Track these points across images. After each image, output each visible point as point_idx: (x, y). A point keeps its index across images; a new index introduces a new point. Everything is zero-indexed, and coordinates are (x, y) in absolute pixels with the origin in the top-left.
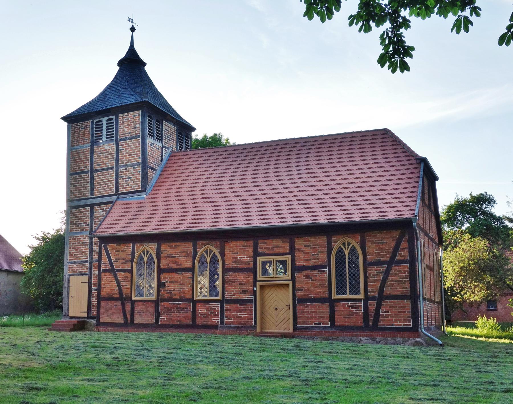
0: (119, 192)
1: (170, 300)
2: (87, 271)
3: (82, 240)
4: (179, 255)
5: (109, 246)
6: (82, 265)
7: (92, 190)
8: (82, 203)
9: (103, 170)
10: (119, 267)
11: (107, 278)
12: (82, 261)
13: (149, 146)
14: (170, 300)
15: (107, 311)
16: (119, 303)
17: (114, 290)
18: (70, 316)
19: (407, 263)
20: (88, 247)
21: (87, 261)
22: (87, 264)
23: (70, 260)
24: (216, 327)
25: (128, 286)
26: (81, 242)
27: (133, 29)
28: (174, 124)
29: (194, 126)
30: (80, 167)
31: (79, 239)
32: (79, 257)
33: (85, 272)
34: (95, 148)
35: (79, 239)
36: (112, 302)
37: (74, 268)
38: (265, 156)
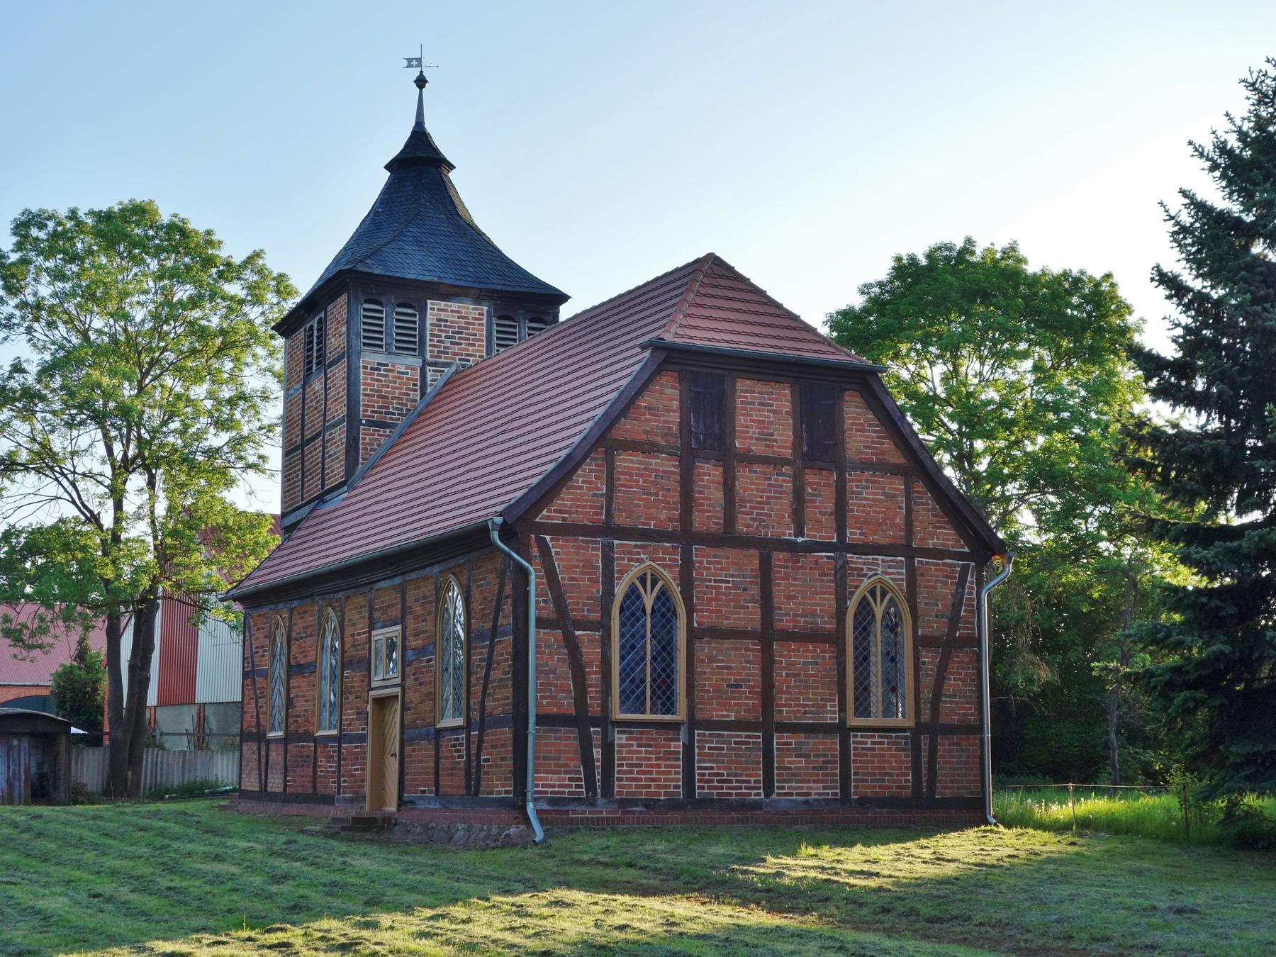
27: (421, 82)
28: (478, 300)
29: (564, 289)
38: (617, 342)
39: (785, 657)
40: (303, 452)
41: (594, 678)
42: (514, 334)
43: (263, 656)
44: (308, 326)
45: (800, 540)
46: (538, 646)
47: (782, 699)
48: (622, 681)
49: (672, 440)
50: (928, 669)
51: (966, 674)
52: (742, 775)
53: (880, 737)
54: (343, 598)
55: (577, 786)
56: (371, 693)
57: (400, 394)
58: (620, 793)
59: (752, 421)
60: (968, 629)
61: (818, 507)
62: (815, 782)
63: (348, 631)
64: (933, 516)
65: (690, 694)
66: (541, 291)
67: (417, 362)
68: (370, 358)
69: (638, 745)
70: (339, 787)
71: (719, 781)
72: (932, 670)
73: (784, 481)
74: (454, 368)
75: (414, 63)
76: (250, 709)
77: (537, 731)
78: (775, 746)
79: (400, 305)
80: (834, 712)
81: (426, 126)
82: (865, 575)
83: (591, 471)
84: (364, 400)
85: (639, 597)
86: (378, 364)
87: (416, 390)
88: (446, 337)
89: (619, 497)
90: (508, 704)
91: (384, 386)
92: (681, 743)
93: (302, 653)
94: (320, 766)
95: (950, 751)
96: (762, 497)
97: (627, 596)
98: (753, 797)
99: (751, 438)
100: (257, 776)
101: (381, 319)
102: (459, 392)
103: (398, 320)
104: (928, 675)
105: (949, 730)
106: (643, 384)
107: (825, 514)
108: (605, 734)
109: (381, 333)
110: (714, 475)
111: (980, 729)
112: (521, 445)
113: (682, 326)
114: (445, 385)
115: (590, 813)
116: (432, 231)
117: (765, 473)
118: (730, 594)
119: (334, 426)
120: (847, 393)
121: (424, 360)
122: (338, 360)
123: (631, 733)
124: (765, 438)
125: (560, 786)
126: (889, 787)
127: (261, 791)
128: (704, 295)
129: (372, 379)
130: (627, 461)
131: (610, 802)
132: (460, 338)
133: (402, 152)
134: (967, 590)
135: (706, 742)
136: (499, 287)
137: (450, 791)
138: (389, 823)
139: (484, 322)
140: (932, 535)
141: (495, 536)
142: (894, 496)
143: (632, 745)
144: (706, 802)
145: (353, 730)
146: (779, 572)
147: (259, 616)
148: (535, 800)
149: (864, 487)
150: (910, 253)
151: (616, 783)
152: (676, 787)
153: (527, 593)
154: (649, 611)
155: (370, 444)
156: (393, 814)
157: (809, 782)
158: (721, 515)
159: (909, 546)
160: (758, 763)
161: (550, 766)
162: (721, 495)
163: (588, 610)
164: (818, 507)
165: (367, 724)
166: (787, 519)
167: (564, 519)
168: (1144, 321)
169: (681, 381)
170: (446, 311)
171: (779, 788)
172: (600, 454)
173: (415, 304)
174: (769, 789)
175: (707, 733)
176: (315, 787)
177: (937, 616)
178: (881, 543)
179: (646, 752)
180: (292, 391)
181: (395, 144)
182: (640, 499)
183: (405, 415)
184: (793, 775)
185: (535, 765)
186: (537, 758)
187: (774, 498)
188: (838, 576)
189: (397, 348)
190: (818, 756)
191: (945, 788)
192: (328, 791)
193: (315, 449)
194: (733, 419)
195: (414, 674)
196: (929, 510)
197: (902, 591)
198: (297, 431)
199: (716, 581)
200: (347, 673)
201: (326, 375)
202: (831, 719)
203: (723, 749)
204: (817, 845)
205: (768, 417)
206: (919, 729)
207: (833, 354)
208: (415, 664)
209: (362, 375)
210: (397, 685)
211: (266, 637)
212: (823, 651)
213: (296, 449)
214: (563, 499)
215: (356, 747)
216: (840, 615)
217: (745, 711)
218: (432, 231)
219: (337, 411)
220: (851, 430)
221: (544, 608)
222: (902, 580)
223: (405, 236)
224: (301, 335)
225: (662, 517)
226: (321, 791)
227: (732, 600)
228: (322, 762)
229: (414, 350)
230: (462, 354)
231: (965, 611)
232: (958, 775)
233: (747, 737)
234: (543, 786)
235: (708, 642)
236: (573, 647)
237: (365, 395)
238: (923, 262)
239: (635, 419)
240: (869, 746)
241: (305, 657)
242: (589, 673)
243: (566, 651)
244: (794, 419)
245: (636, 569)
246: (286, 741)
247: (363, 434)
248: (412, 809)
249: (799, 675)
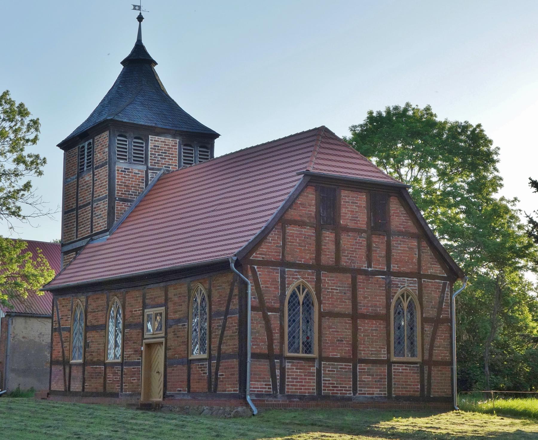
4: (98, 309)
13: (118, 173)
19: (237, 314)
24: (115, 395)
27: (140, 18)
28: (174, 136)
34: (81, 180)
39: (363, 326)
40: (77, 213)
41: (277, 336)
42: (192, 154)
43: (67, 320)
44: (81, 146)
45: (370, 269)
46: (252, 320)
47: (361, 347)
48: (289, 337)
49: (312, 220)
50: (427, 333)
51: (445, 336)
52: (343, 384)
53: (406, 366)
54: (124, 292)
55: (269, 388)
56: (144, 341)
57: (135, 184)
58: (288, 392)
59: (348, 211)
60: (446, 314)
61: (378, 254)
62: (376, 388)
63: (128, 309)
64: (431, 258)
65: (320, 345)
66: (205, 132)
67: (144, 168)
68: (121, 165)
69: (296, 369)
70: (122, 389)
71: (332, 387)
72: (429, 334)
73: (362, 240)
74: (162, 171)
75: (137, 8)
76: (58, 348)
77: (251, 361)
78: (358, 370)
79: (136, 138)
80: (385, 354)
81: (143, 42)
82: (399, 287)
83: (275, 234)
84: (117, 187)
85: (297, 296)
86: (125, 169)
87: (143, 183)
88: (158, 155)
89: (288, 247)
90: (236, 348)
91: (127, 180)
92: (315, 368)
93: (95, 319)
94: (109, 378)
95: (437, 373)
96: (353, 248)
97: (291, 296)
98: (348, 395)
99: (348, 219)
100: (63, 383)
101: (126, 145)
102: (169, 186)
103: (134, 146)
104: (427, 336)
105: (437, 363)
106: (300, 192)
107: (381, 257)
108: (281, 363)
109: (126, 152)
110: (331, 237)
111: (451, 363)
112: (226, 219)
113: (316, 164)
114: (158, 180)
115: (275, 401)
116: (150, 99)
117: (354, 237)
118: (338, 295)
119: (100, 200)
120: (392, 197)
121: (147, 167)
122: (102, 166)
123: (293, 363)
124: (354, 219)
125: (261, 388)
126: (409, 391)
127: (66, 390)
128: (323, 148)
129: (121, 177)
130: (291, 230)
131: (283, 396)
132: (165, 156)
133: (130, 56)
134: (445, 295)
135: (327, 368)
136: (185, 130)
137: (198, 390)
138: (159, 406)
139: (177, 147)
140: (430, 268)
141: (232, 265)
142: (412, 248)
143: (293, 369)
144: (327, 397)
145: (131, 359)
146: (360, 285)
147: (64, 299)
148: (251, 395)
149: (399, 244)
150: (378, 110)
151: (286, 387)
152: (313, 389)
153: (247, 294)
154: (301, 303)
155: (120, 211)
156: (160, 402)
157: (373, 388)
158: (334, 257)
159: (419, 273)
160: (350, 378)
161: (257, 378)
162: (334, 247)
163: (274, 303)
164: (378, 254)
165: (142, 356)
166: (364, 259)
167: (263, 258)
168: (499, 149)
169: (316, 190)
170: (158, 141)
171: (360, 391)
172: (279, 226)
173: (143, 138)
174: (355, 390)
175: (327, 363)
176: (105, 388)
177: (432, 308)
178: (406, 271)
179: (300, 372)
180: (69, 180)
181: (127, 51)
182: (297, 249)
183: (138, 195)
184: (366, 384)
185: (251, 378)
186: (251, 374)
187: (358, 248)
188: (387, 287)
189: (134, 160)
190: (377, 375)
191: (435, 392)
192: (114, 391)
193: (86, 211)
194: (340, 210)
195: (174, 332)
196: (428, 255)
197: (416, 295)
198: (73, 201)
199: (331, 289)
200: (126, 331)
201: (93, 173)
202: (383, 357)
203: (334, 371)
204: (397, 417)
205: (356, 209)
206: (424, 363)
207: (385, 178)
208: (174, 327)
209: (116, 174)
210: (162, 337)
211: (69, 310)
212: (380, 324)
213: (73, 210)
214: (263, 248)
215: (133, 368)
216: (388, 306)
217: (345, 353)
218: (150, 99)
219: (101, 192)
220: (393, 215)
221: (254, 301)
222: (416, 290)
223: (136, 101)
224: (76, 150)
225: (307, 257)
226: (109, 390)
227: (339, 299)
228: (110, 375)
229: (142, 161)
230: (166, 164)
231: (445, 305)
232: (441, 386)
233: (345, 365)
234: (253, 388)
235: (328, 319)
236: (267, 319)
237: (118, 185)
238: (384, 114)
239: (295, 209)
240: (401, 371)
241: (98, 321)
242: (275, 333)
243: (264, 322)
244: (367, 211)
245: (296, 283)
246: (84, 365)
247: (117, 205)
248: (172, 399)
249: (369, 336)
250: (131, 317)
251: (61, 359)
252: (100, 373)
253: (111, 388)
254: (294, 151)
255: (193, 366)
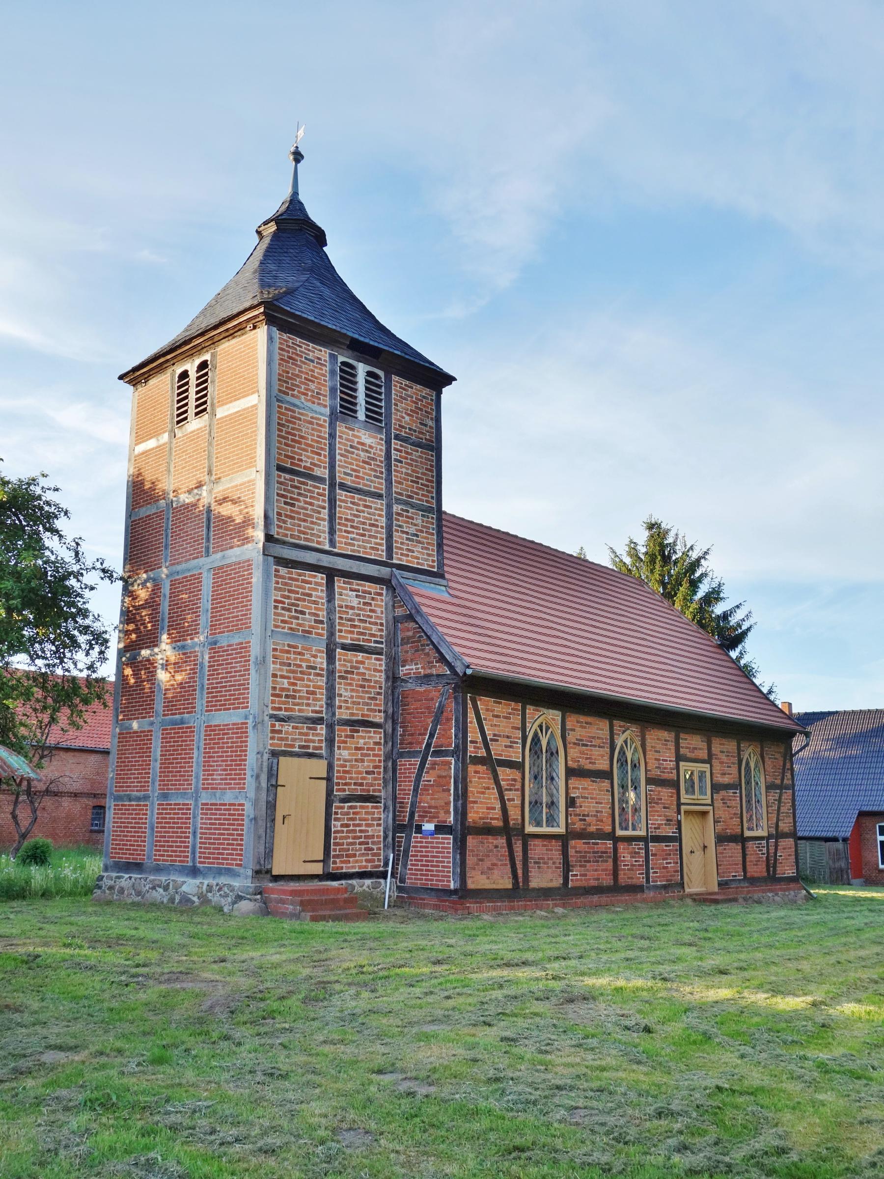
0: (395, 561)
1: (582, 835)
2: (321, 748)
3: (308, 661)
5: (480, 700)
6: (309, 728)
7: (332, 531)
8: (310, 558)
9: (358, 491)
10: (501, 755)
11: (479, 777)
12: (308, 719)
14: (582, 835)
15: (482, 860)
16: (501, 841)
17: (494, 809)
18: (275, 873)
20: (322, 682)
21: (322, 719)
22: (321, 729)
23: (274, 709)
24: (635, 889)
25: (518, 802)
26: (304, 665)
30: (303, 458)
31: (299, 654)
32: (298, 704)
33: (315, 748)
35: (299, 654)
36: (490, 839)
37: (287, 733)
44: (179, 371)
94: (623, 861)
137: (756, 875)
192: (634, 881)
195: (722, 800)
226: (623, 879)
250: (657, 767)
251: (500, 824)
252: (606, 852)
253: (629, 878)
254: (478, 549)
255: (750, 844)
